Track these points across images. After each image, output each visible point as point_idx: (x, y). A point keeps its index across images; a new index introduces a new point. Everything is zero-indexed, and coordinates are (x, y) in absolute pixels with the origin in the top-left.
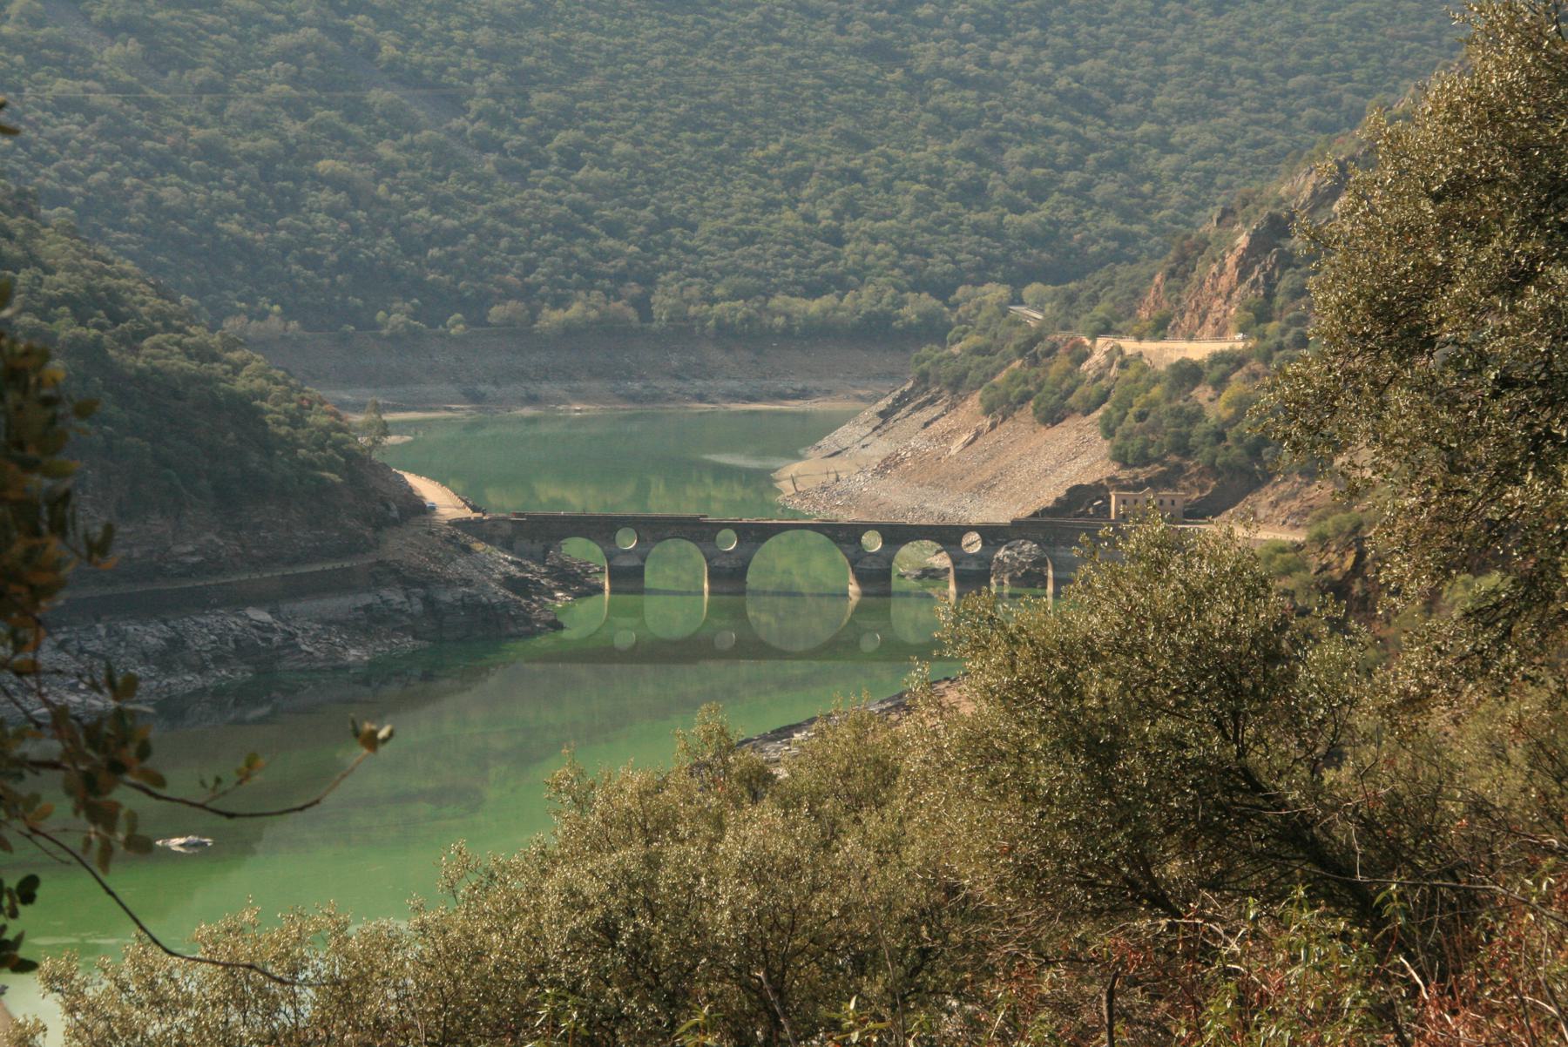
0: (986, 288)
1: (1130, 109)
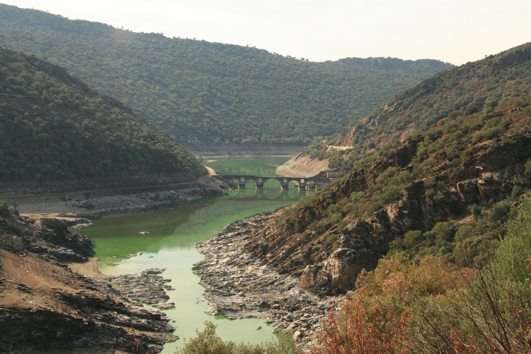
1: (345, 107)
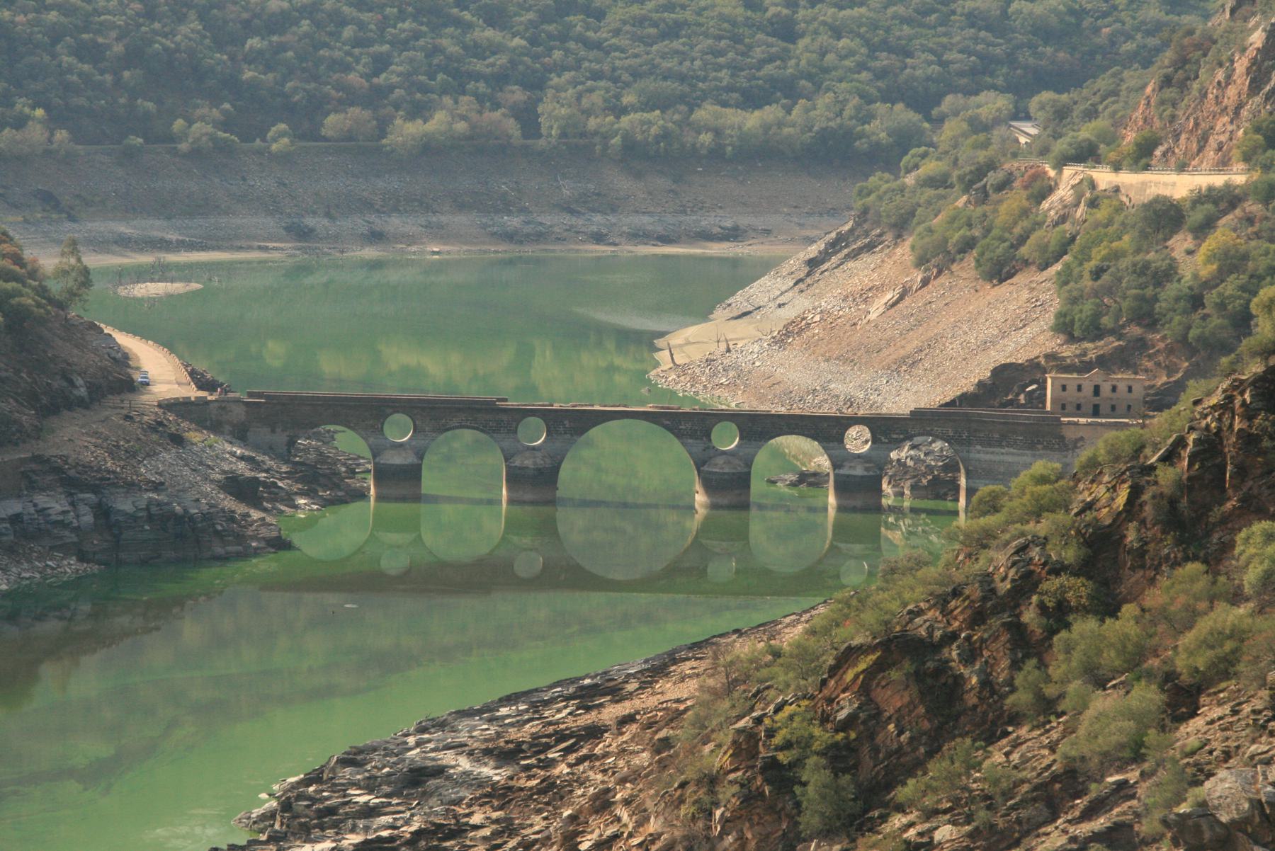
0: (982, 97)
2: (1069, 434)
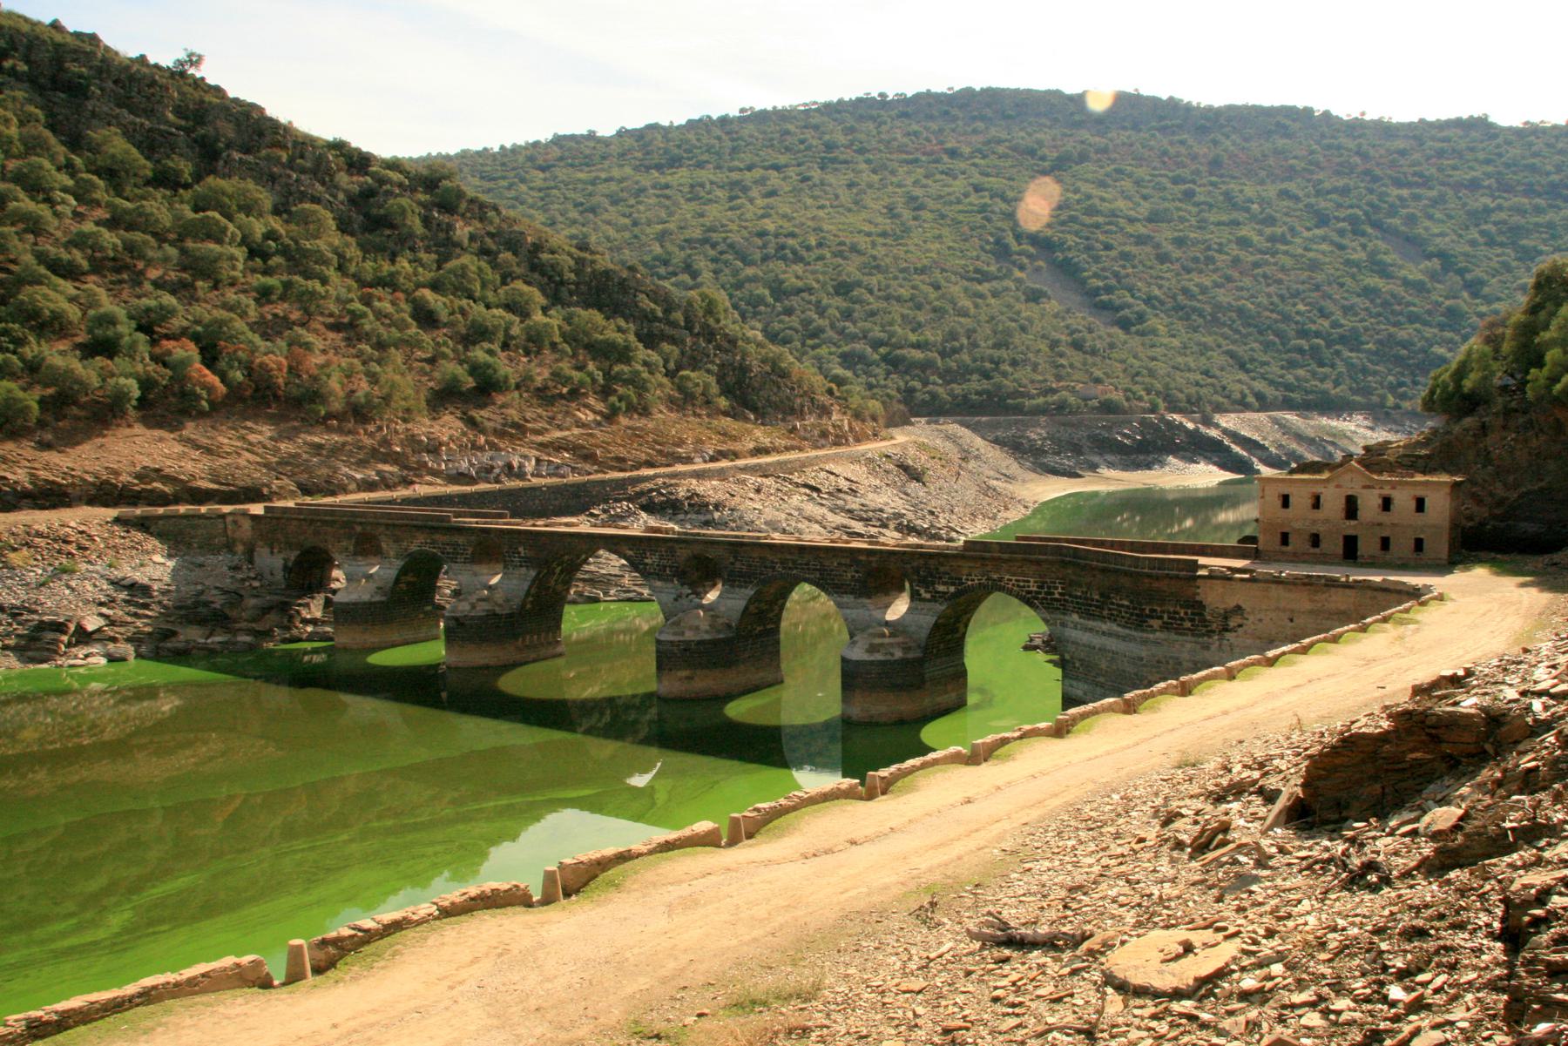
2: (1214, 599)
